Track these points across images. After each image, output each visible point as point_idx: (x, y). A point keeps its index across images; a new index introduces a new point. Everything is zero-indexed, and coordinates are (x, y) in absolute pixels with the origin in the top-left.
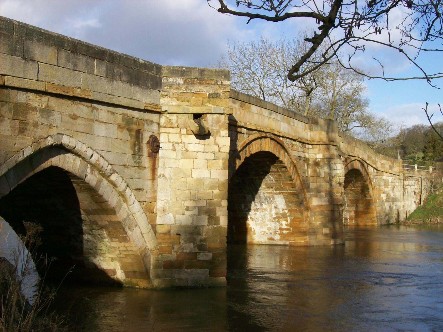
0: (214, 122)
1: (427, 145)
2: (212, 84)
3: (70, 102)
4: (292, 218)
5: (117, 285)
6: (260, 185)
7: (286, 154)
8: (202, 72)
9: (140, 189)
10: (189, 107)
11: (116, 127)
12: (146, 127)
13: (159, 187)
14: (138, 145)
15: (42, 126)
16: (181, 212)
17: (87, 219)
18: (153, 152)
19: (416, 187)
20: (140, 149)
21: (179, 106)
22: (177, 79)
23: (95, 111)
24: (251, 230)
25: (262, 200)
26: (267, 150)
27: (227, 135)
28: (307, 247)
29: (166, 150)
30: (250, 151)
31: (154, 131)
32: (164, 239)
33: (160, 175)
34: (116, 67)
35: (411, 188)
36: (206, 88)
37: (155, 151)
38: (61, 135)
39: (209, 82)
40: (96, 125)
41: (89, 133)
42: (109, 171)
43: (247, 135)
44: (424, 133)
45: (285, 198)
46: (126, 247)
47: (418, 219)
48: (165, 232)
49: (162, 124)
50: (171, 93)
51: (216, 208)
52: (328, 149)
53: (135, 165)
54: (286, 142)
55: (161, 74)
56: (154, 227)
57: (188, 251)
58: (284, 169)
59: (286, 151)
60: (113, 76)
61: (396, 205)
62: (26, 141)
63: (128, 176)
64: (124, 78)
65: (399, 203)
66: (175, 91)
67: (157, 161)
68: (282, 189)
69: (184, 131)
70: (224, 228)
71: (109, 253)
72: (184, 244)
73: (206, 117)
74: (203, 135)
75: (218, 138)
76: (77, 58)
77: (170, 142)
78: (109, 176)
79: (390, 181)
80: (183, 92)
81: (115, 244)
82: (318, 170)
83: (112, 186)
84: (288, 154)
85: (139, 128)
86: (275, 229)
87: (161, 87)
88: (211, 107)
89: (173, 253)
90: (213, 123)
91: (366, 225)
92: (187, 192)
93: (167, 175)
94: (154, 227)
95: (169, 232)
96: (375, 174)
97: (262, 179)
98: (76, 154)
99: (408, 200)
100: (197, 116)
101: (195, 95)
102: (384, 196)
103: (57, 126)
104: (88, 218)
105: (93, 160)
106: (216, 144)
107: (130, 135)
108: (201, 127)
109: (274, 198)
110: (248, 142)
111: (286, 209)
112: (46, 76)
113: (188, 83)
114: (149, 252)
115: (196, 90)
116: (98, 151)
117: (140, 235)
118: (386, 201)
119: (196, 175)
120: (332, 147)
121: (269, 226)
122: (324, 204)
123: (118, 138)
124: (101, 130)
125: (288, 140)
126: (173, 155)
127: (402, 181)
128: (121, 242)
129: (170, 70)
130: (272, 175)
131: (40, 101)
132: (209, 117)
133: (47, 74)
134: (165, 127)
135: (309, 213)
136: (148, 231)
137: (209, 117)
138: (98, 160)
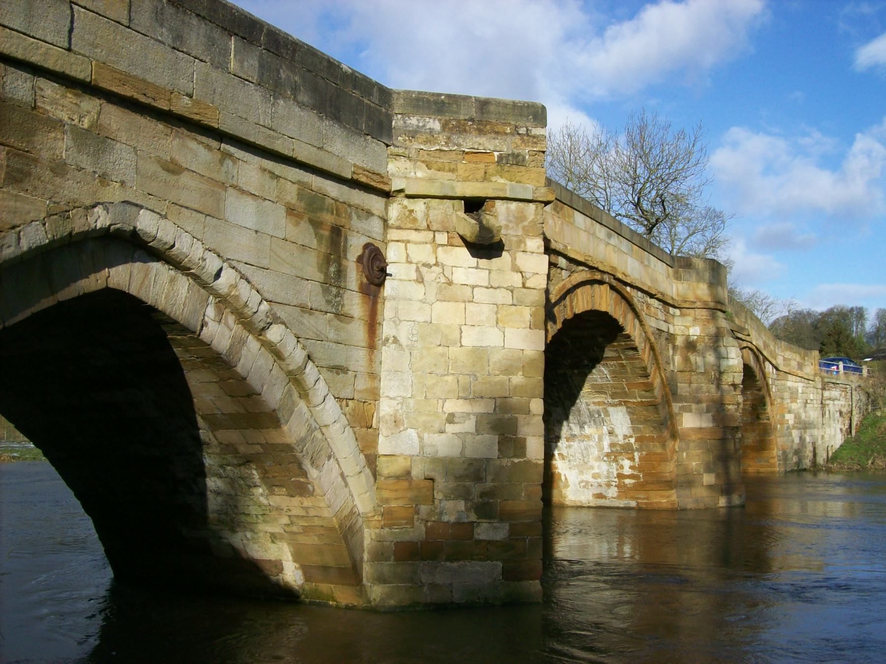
0: (511, 218)
1: (825, 341)
2: (506, 134)
3: (161, 126)
4: (644, 453)
5: (288, 597)
6: (580, 388)
7: (636, 321)
8: (484, 105)
9: (339, 369)
10: (455, 184)
11: (282, 211)
12: (355, 222)
13: (385, 366)
14: (335, 261)
15: (79, 174)
16: (437, 426)
17: (213, 439)
18: (371, 282)
19: (843, 403)
20: (340, 273)
21: (431, 180)
22: (427, 120)
23: (229, 162)
24: (560, 479)
25: (583, 419)
26: (603, 309)
28: (676, 511)
29: (400, 280)
30: (572, 308)
31: (374, 236)
32: (396, 491)
33: (387, 340)
34: (284, 67)
35: (834, 404)
36: (492, 141)
37: (377, 281)
38: (134, 209)
39: (499, 128)
40: (231, 199)
41: (212, 213)
42: (263, 317)
43: (568, 273)
44: (812, 323)
45: (629, 413)
46: (306, 509)
47: (850, 461)
48: (398, 473)
49: (391, 222)
50: (413, 151)
51: (517, 418)
52: (714, 318)
53: (329, 308)
54: (637, 297)
55: (390, 106)
56: (372, 461)
57: (452, 519)
58: (631, 353)
59: (637, 315)
60: (276, 87)
61: (811, 435)
62: (27, 207)
63: (311, 335)
64: (303, 97)
65: (815, 432)
66: (422, 147)
67: (379, 306)
68: (625, 394)
69: (442, 238)
70: (536, 464)
71: (265, 521)
72: (444, 503)
73: (493, 207)
74: (486, 247)
75: (519, 255)
76: (183, 22)
77: (411, 263)
78: (263, 329)
79: (800, 391)
80: (441, 150)
81: (279, 499)
82: (693, 358)
83: (270, 358)
84: (641, 322)
85: (339, 223)
86: (608, 477)
87: (390, 136)
88: (506, 184)
89: (417, 523)
90: (511, 222)
91: (759, 473)
92: (450, 379)
93: (403, 340)
94: (372, 461)
95: (408, 473)
96: (775, 376)
97: (586, 375)
98: (177, 265)
99: (829, 426)
100: (474, 205)
101: (467, 157)
102: (790, 418)
103: (123, 183)
104: (215, 437)
105: (223, 284)
106: (516, 269)
107: (316, 235)
108: (485, 230)
109: (607, 414)
110: (569, 286)
111: (631, 437)
112: (94, 45)
113: (451, 129)
114: (360, 520)
115: (470, 145)
116: (234, 263)
117: (340, 479)
118: (794, 428)
119: (470, 339)
120: (720, 314)
121: (596, 471)
122: (704, 425)
123: (288, 237)
124: (243, 212)
125: (640, 294)
126: (418, 291)
127: (820, 391)
128: (292, 496)
129: (411, 99)
130: (606, 365)
131: (74, 108)
132: (500, 207)
133: (98, 41)
134: (399, 228)
135: (677, 445)
136: (358, 469)
137: (500, 207)
138: (234, 286)
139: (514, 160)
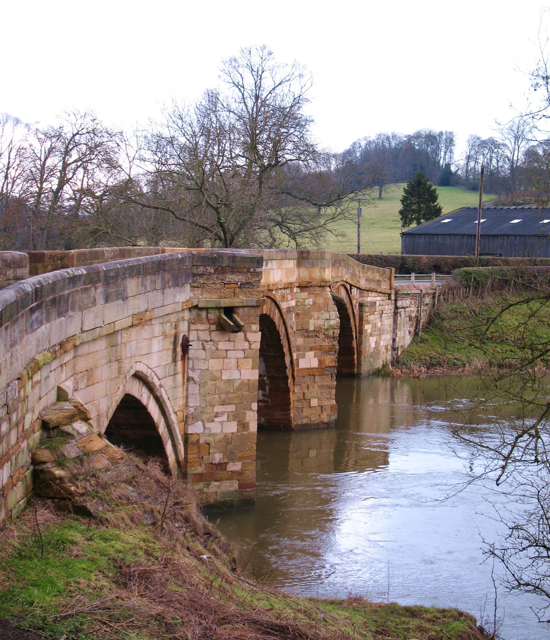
27: (258, 329)
106: (246, 340)
111: (265, 376)
132: (240, 311)
139: (248, 284)
